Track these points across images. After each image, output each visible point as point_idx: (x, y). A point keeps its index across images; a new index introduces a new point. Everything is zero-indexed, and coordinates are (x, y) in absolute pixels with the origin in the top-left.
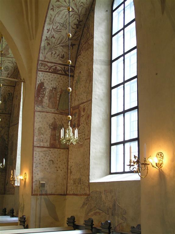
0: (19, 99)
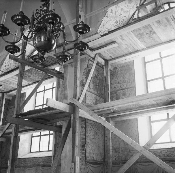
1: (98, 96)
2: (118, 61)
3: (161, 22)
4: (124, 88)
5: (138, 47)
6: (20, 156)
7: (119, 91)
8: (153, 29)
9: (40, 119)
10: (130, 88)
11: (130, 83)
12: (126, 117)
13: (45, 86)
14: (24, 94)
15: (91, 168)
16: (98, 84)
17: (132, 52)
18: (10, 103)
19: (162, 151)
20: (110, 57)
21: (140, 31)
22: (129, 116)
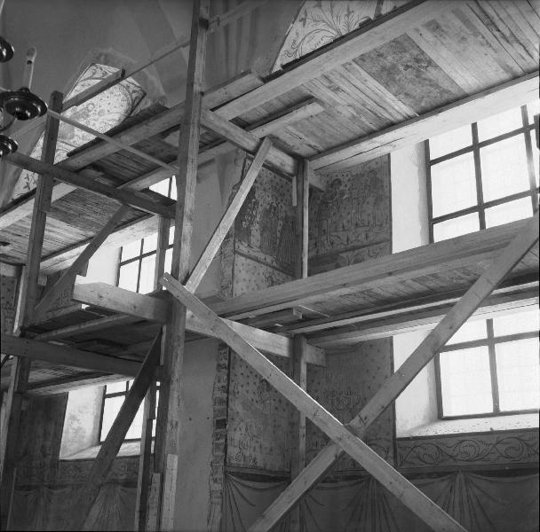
0: (107, 454)
1: (278, 270)
2: (337, 160)
3: (443, 28)
4: (356, 244)
5: (390, 114)
6: (69, 453)
7: (344, 255)
8: (423, 53)
9: (95, 342)
10: (377, 243)
11: (376, 229)
12: (352, 333)
13: (143, 240)
15: (245, 491)
16: (278, 234)
17: (374, 128)
19: (464, 441)
20: (310, 146)
21: (381, 58)
22: (357, 332)
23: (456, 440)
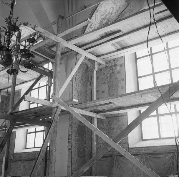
14: (19, 92)
18: (6, 99)
23: (23, 154)
